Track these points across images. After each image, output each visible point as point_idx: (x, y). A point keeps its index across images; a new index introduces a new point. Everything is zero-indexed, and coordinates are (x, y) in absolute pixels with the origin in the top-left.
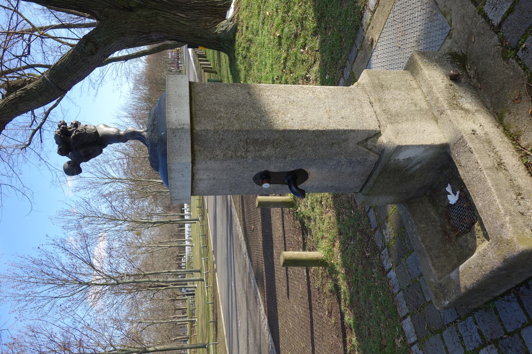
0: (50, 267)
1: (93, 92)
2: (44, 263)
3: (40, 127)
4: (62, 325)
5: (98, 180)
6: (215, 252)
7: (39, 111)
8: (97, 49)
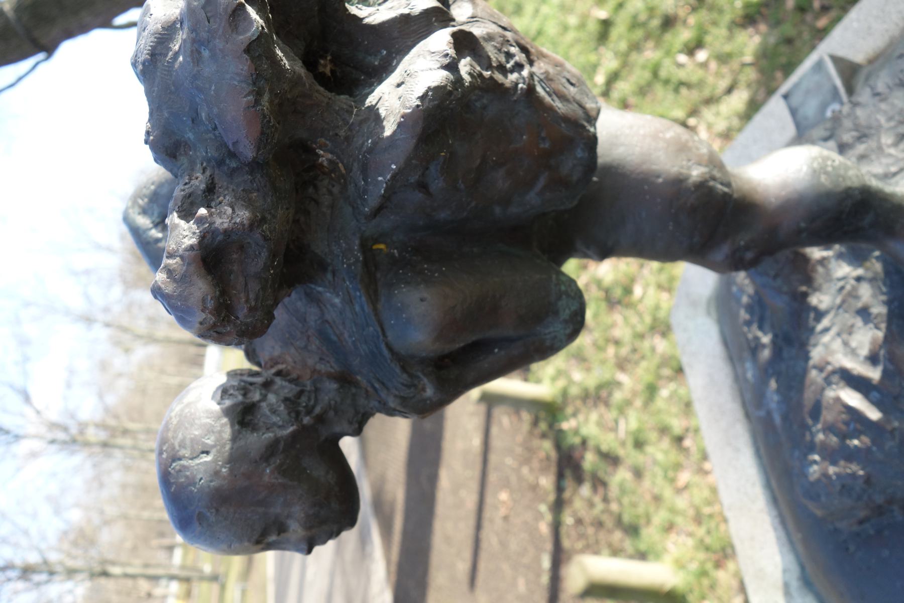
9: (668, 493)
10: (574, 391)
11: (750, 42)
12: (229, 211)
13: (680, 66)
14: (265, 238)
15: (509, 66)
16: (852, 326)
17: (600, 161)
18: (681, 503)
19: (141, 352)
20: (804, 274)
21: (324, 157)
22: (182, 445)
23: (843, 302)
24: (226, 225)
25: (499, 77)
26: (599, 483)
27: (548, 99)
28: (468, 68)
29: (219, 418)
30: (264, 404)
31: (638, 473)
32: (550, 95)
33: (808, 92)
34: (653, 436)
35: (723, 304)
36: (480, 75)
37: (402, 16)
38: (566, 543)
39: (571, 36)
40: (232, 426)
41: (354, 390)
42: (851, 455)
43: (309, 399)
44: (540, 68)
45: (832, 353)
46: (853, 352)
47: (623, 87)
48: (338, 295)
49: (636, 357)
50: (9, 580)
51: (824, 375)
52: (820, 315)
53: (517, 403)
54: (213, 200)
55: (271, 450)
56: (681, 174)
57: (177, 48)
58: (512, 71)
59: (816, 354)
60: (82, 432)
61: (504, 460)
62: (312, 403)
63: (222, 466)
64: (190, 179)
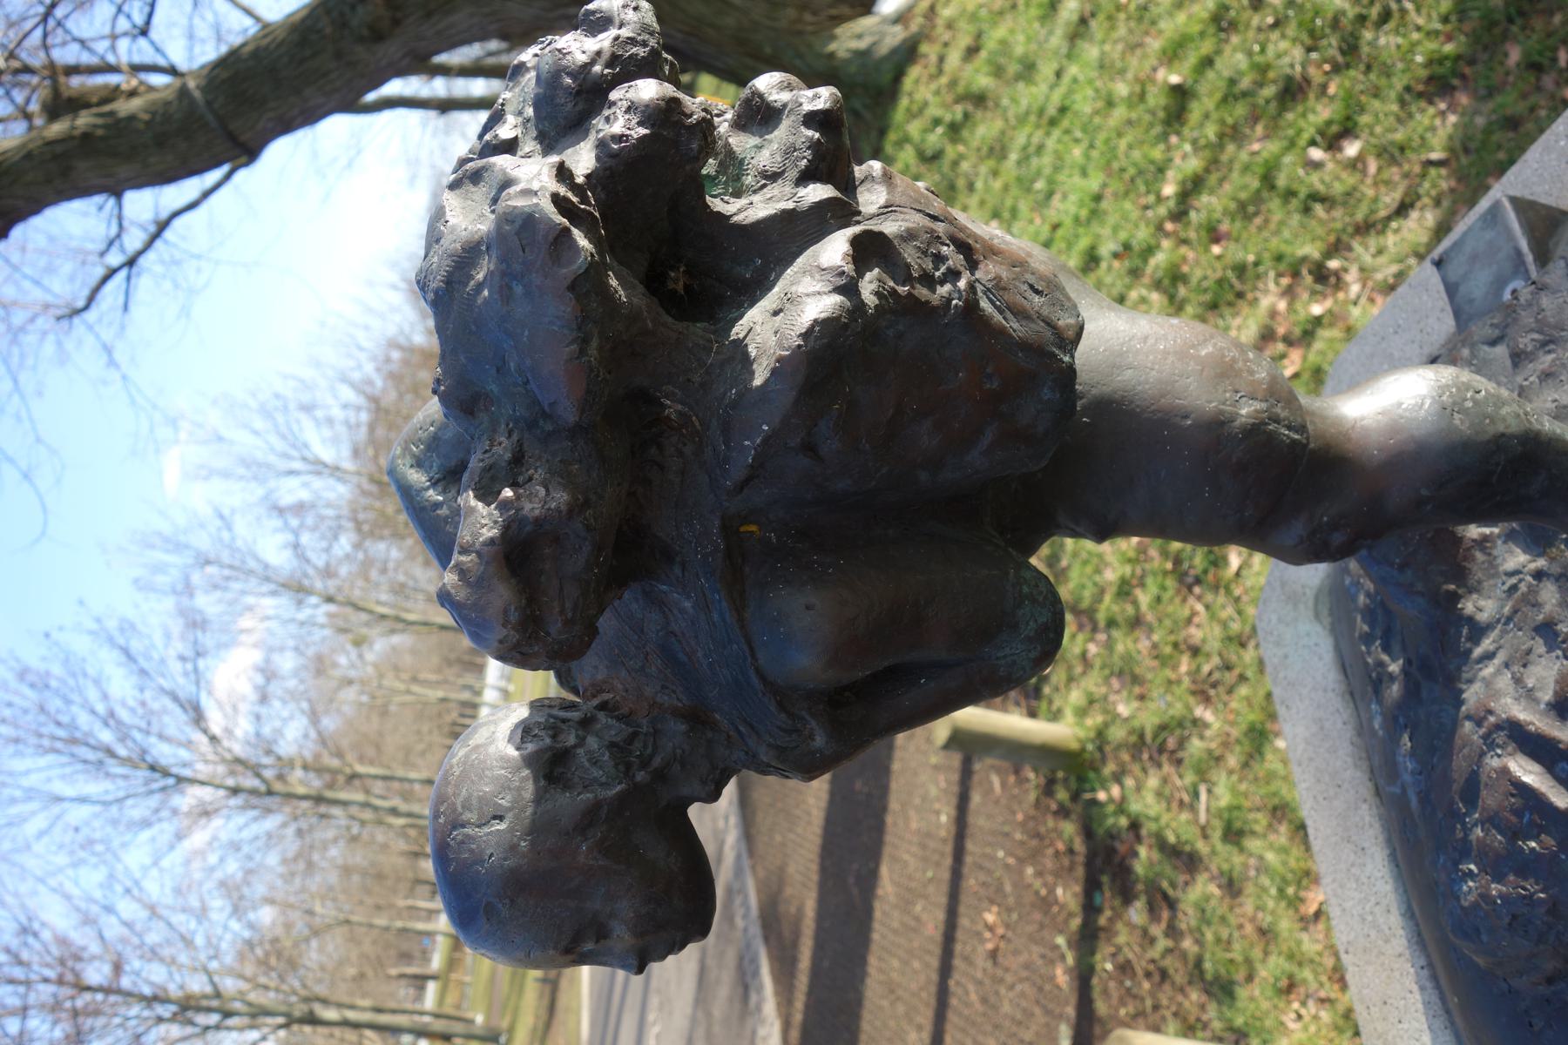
0: (68, 702)
2: (54, 683)
3: (131, 263)
4: (69, 887)
5: (272, 459)
7: (142, 204)
8: (396, 22)
9: (1285, 924)
10: (1117, 733)
11: (1438, 127)
12: (542, 492)
13: (1317, 166)
14: (588, 528)
15: (937, 274)
16: (1529, 652)
18: (1310, 944)
19: (381, 645)
20: (1456, 566)
21: (672, 409)
22: (467, 806)
23: (1515, 611)
24: (537, 512)
25: (922, 292)
26: (1162, 901)
27: (998, 317)
28: (874, 286)
29: (519, 769)
30: (581, 751)
31: (1232, 887)
32: (1001, 312)
33: (1474, 258)
34: (1260, 820)
35: (1337, 602)
36: (894, 292)
37: (784, 211)
38: (1101, 1007)
39: (1120, 113)
40: (536, 780)
41: (710, 735)
42: (1525, 866)
43: (645, 746)
44: (987, 271)
45: (1496, 695)
46: (1529, 695)
47: (1209, 204)
48: (689, 597)
49: (1230, 677)
50: (160, 1020)
51: (1482, 731)
52: (1478, 631)
53: (1016, 752)
54: (521, 473)
55: (589, 818)
56: (1222, 412)
57: (480, 276)
58: (942, 283)
59: (1472, 695)
60: (281, 777)
61: (992, 852)
62: (649, 751)
63: (520, 839)
64: (492, 445)
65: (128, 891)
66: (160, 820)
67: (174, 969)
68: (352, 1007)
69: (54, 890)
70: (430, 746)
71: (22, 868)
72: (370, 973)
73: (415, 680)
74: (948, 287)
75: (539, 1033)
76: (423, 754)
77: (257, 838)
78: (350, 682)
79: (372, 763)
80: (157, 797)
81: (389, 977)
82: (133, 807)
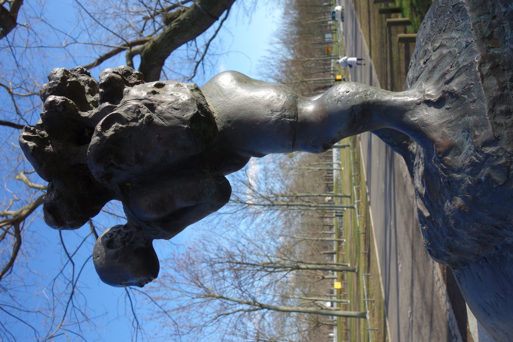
1: (247, 20)
3: (202, 58)
4: (228, 237)
6: (368, 183)
7: (201, 40)
17: (410, 44)
55: (116, 255)
60: (276, 200)
65: (242, 236)
66: (246, 216)
67: (259, 256)
68: (310, 264)
69: (224, 238)
70: (320, 184)
71: (215, 233)
72: (315, 254)
73: (310, 165)
74: (142, 119)
75: (367, 267)
76: (318, 187)
77: (274, 218)
78: (292, 169)
79: (303, 192)
80: (244, 211)
81: (321, 254)
82: (240, 213)
